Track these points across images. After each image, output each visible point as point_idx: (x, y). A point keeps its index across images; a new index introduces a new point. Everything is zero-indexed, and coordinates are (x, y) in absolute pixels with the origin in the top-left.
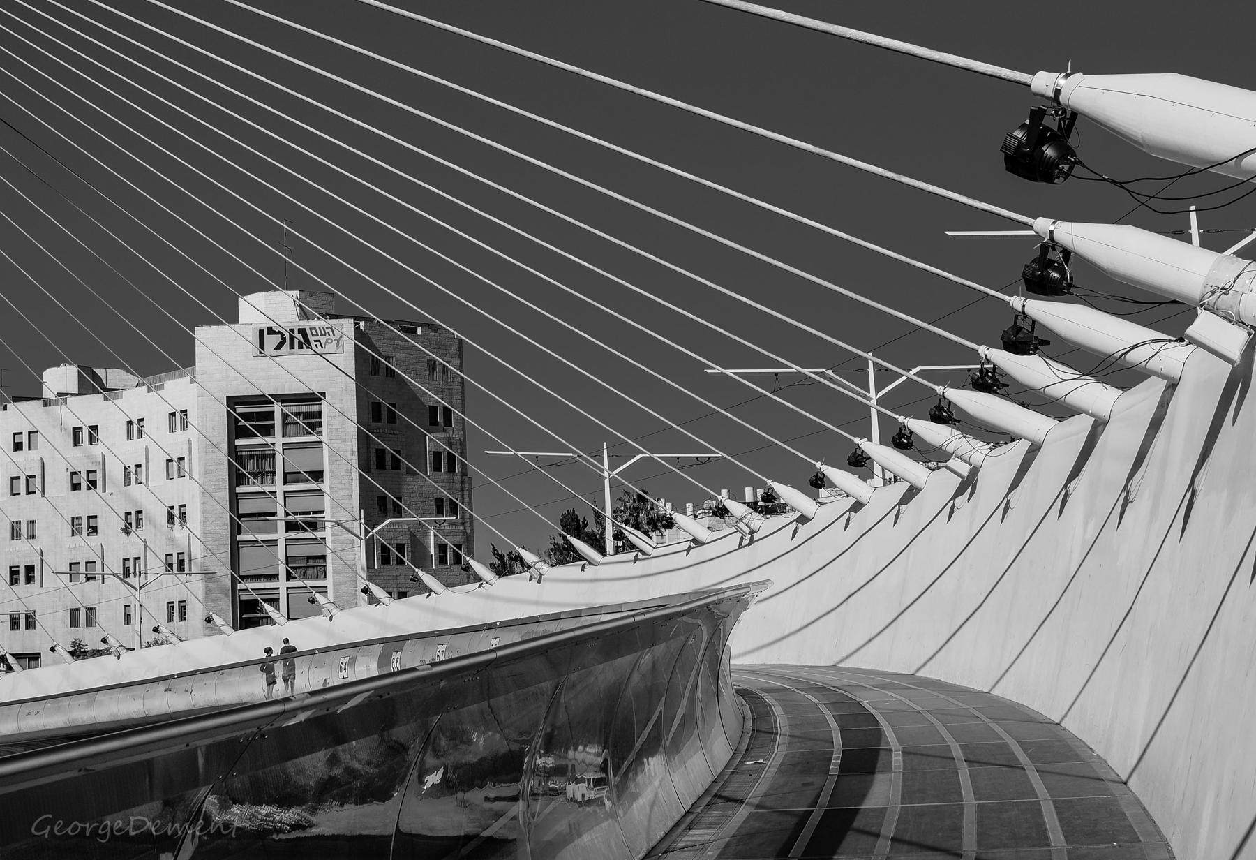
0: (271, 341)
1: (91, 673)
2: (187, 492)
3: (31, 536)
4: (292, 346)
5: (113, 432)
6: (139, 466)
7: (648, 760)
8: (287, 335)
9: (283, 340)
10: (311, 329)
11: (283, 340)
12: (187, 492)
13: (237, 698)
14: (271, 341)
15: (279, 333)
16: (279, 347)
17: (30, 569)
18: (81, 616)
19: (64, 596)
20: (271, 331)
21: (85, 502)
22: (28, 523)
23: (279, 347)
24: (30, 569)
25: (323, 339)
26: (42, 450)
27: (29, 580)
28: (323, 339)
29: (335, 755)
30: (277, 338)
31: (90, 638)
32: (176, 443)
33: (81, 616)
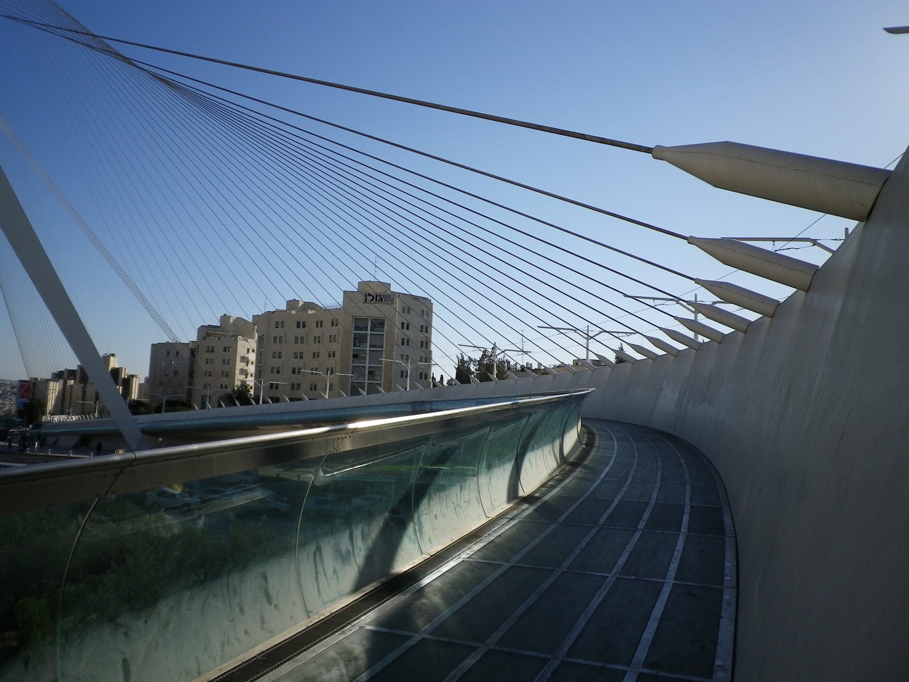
1: (297, 405)
2: (336, 347)
3: (280, 357)
4: (376, 301)
6: (319, 337)
7: (490, 483)
8: (375, 296)
9: (373, 297)
10: (383, 296)
11: (373, 297)
12: (336, 347)
13: (274, 584)
14: (369, 298)
15: (372, 295)
16: (372, 300)
17: (302, 338)
18: (293, 387)
19: (276, 400)
20: (369, 295)
21: (298, 347)
22: (279, 352)
23: (372, 300)
24: (302, 338)
25: (387, 299)
28: (387, 299)
29: (306, 678)
30: (372, 297)
31: (296, 394)
32: (334, 330)
33: (293, 387)
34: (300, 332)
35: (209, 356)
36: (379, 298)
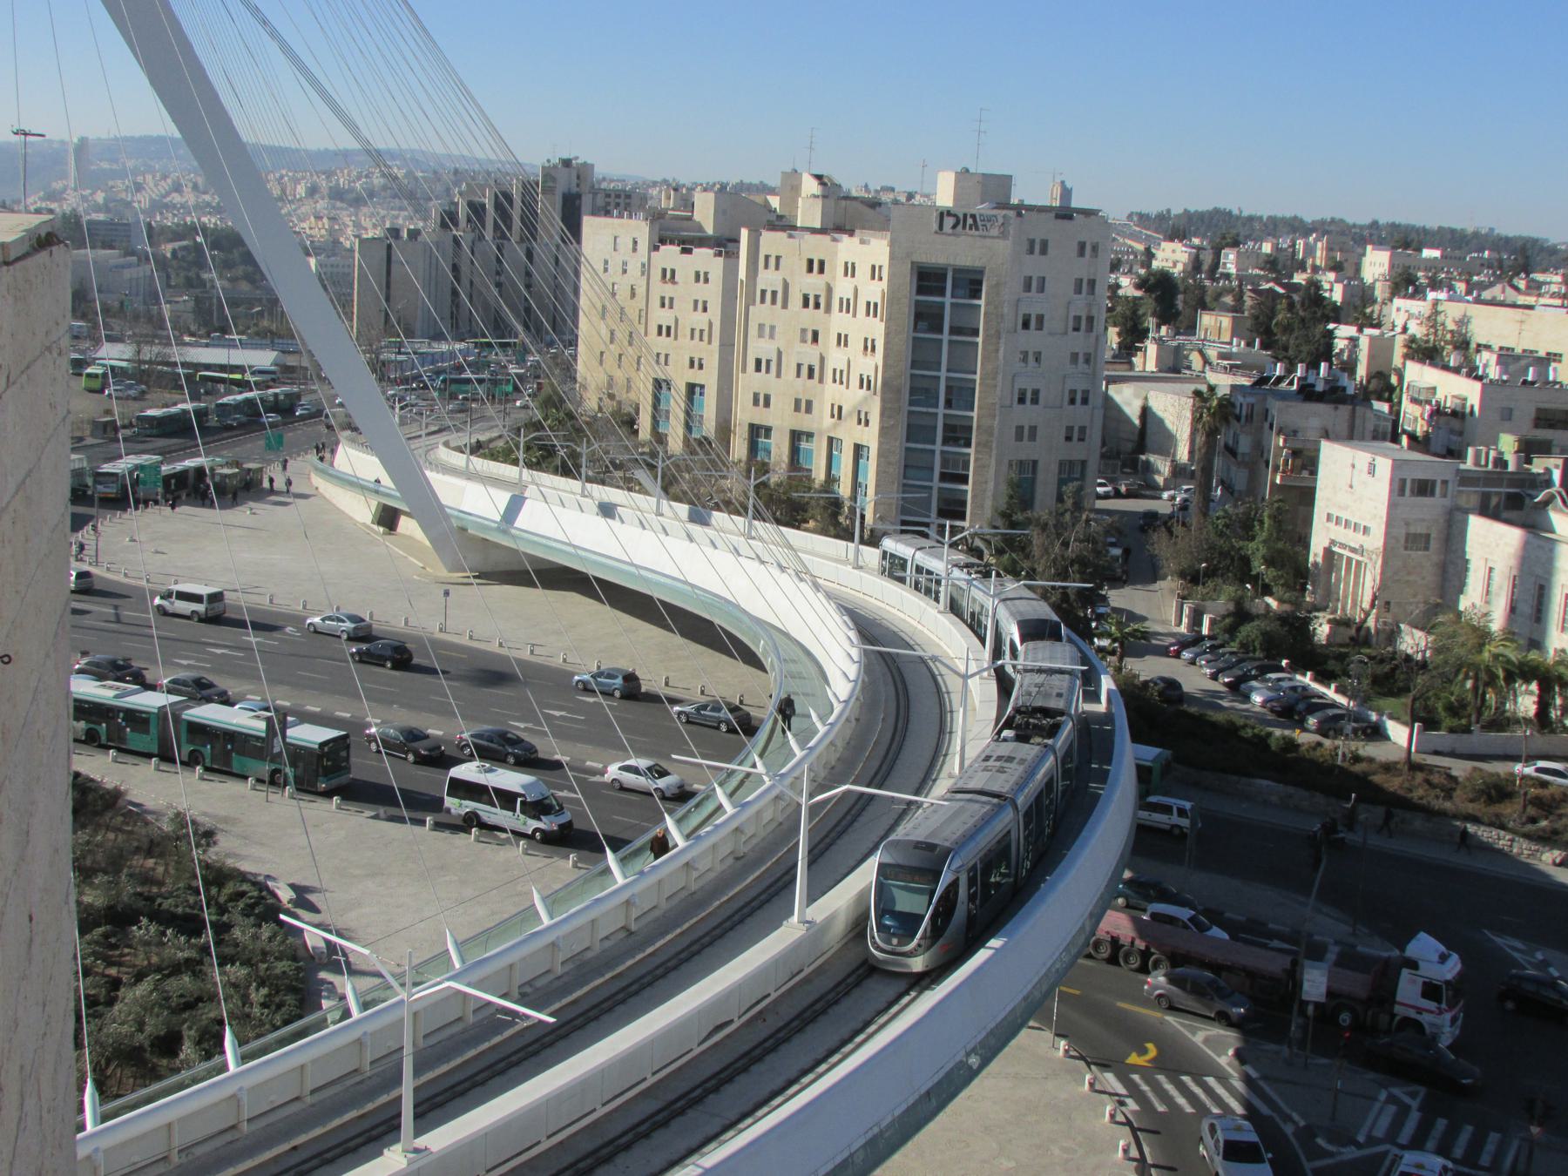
0: (949, 222)
5: (836, 271)
14: (949, 222)
16: (954, 227)
26: (779, 342)
27: (811, 375)
34: (814, 284)
35: (668, 290)
36: (970, 221)
